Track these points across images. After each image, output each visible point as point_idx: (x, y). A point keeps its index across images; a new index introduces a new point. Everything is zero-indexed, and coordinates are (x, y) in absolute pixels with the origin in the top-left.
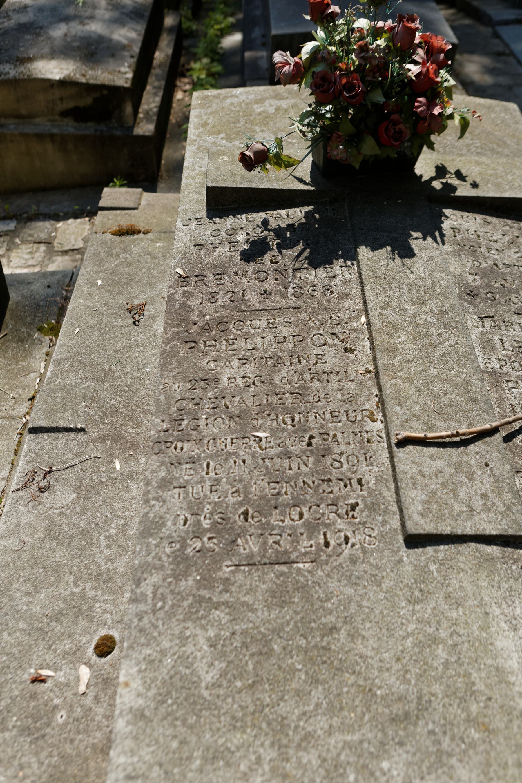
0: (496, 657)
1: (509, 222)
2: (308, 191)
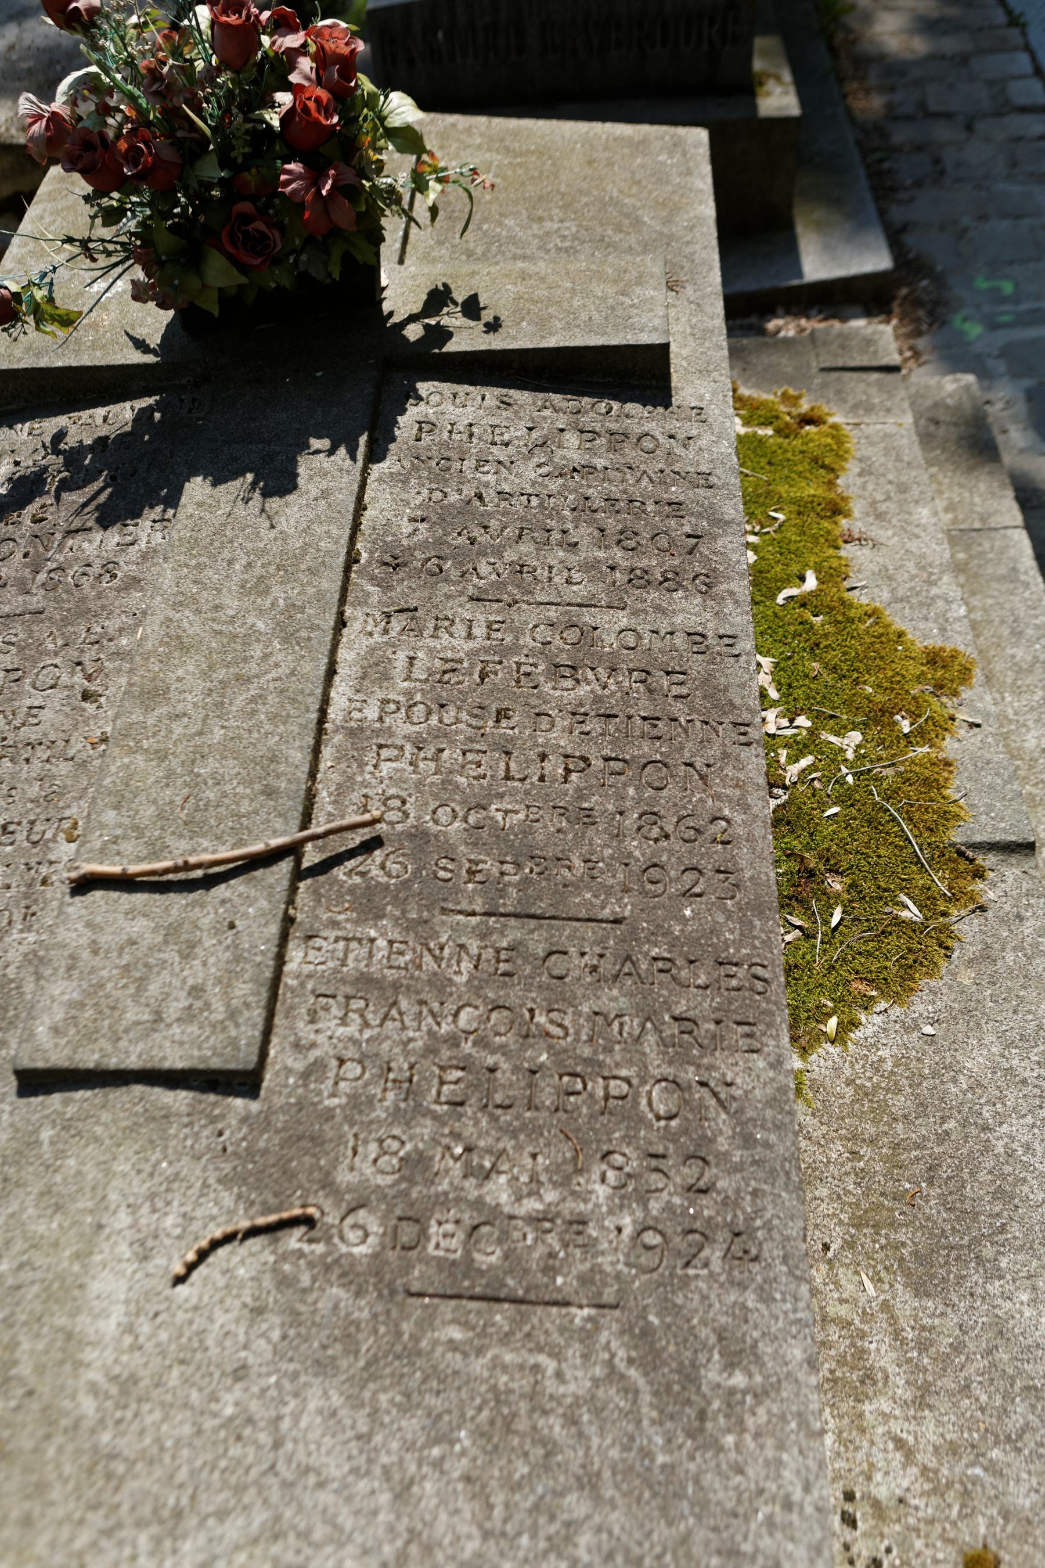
0: (73, 1314)
1: (556, 398)
2: (146, 366)
